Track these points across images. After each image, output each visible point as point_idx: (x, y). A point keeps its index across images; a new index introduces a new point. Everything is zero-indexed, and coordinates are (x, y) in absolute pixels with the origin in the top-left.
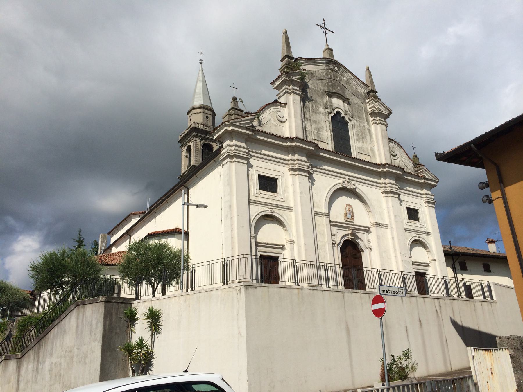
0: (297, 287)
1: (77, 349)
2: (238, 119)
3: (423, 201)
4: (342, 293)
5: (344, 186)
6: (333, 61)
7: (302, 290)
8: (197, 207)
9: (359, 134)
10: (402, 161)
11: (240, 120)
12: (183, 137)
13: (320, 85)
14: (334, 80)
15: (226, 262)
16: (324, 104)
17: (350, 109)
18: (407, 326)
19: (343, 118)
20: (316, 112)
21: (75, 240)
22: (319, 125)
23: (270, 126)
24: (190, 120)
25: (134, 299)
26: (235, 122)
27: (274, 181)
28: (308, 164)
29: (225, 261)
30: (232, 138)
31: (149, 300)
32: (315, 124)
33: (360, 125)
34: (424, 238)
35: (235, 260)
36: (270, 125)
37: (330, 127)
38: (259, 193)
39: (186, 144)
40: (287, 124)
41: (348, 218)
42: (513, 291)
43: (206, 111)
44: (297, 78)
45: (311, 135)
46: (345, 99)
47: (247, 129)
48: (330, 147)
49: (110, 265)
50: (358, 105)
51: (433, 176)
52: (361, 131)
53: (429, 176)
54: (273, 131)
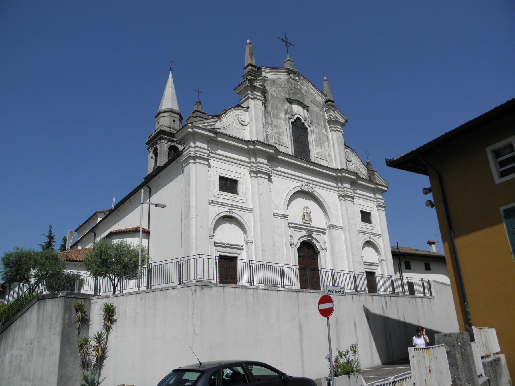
0: (252, 287)
1: (37, 341)
2: (201, 121)
3: (374, 205)
4: (296, 293)
5: (303, 188)
6: (294, 71)
7: (257, 290)
8: (156, 207)
9: (318, 140)
10: (357, 167)
11: (202, 122)
12: (151, 139)
13: (281, 92)
14: (295, 88)
15: (182, 262)
16: (284, 110)
17: (309, 116)
18: (356, 322)
19: (303, 124)
20: (277, 117)
21: (46, 236)
22: (280, 130)
23: (232, 129)
24: (158, 123)
25: (93, 296)
26: (198, 124)
27: (235, 182)
28: (268, 167)
29: (181, 261)
30: (195, 139)
31: (107, 297)
32: (276, 128)
33: (319, 131)
34: (375, 239)
35: (191, 260)
36: (232, 128)
37: (290, 132)
38: (220, 194)
39: (152, 146)
40: (247, 128)
41: (306, 220)
42: (450, 288)
43: (174, 115)
44: (260, 85)
45: (272, 139)
46: (304, 106)
47: (209, 131)
48: (290, 151)
49: (75, 261)
50: (317, 112)
51: (384, 182)
52: (319, 137)
53: (380, 182)
54: (235, 134)
